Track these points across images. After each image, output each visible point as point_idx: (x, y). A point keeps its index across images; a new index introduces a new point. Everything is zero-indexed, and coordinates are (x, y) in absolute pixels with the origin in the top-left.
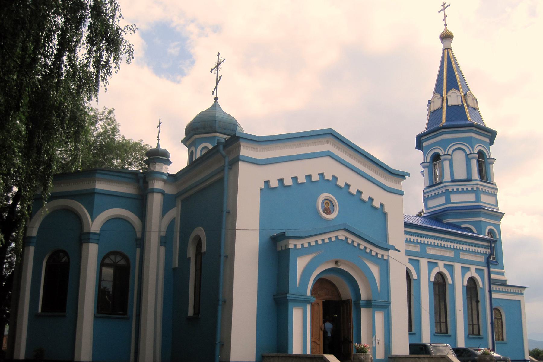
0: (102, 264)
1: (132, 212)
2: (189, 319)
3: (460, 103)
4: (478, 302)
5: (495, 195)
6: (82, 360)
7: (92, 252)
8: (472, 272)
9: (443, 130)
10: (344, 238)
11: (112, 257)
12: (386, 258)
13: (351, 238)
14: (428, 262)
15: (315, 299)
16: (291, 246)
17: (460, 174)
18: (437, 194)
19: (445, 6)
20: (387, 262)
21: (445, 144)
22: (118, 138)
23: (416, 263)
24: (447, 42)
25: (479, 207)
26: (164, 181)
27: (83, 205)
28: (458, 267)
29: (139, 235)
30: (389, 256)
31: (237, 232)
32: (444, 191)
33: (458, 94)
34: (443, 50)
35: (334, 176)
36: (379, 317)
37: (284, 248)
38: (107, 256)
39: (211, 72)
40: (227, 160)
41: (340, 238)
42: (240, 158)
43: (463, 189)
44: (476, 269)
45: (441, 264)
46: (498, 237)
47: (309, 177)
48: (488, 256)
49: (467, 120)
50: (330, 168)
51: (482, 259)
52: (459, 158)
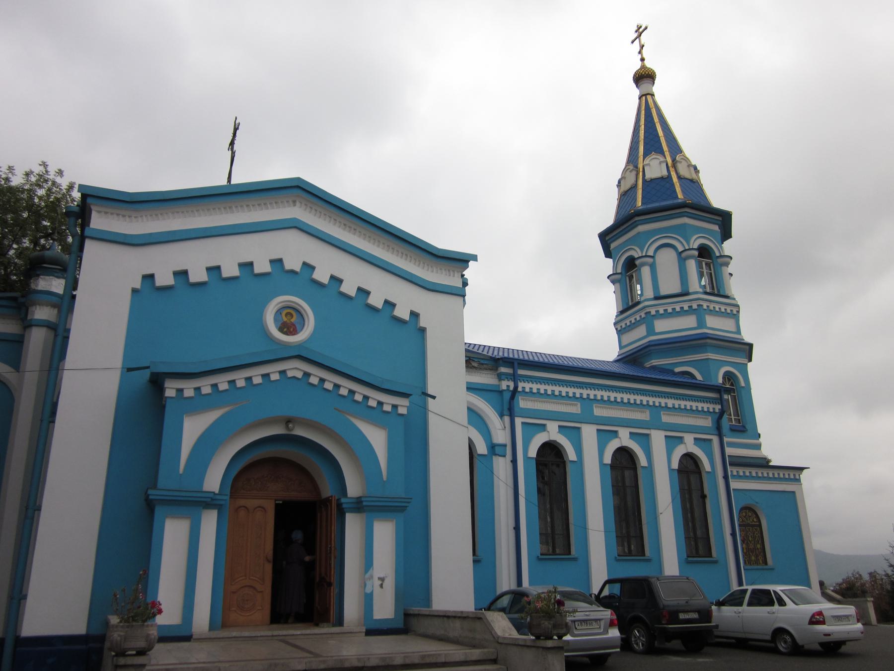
3: (665, 173)
4: (704, 497)
5: (735, 316)
6: (375, 618)
8: (689, 445)
9: (637, 219)
13: (316, 374)
14: (598, 430)
17: (670, 284)
18: (633, 321)
19: (641, 30)
21: (640, 240)
24: (645, 86)
25: (705, 337)
28: (658, 438)
32: (643, 316)
33: (662, 159)
34: (640, 98)
36: (385, 533)
41: (290, 374)
43: (674, 309)
46: (743, 384)
48: (717, 416)
50: (295, 250)
51: (707, 422)
52: (667, 261)
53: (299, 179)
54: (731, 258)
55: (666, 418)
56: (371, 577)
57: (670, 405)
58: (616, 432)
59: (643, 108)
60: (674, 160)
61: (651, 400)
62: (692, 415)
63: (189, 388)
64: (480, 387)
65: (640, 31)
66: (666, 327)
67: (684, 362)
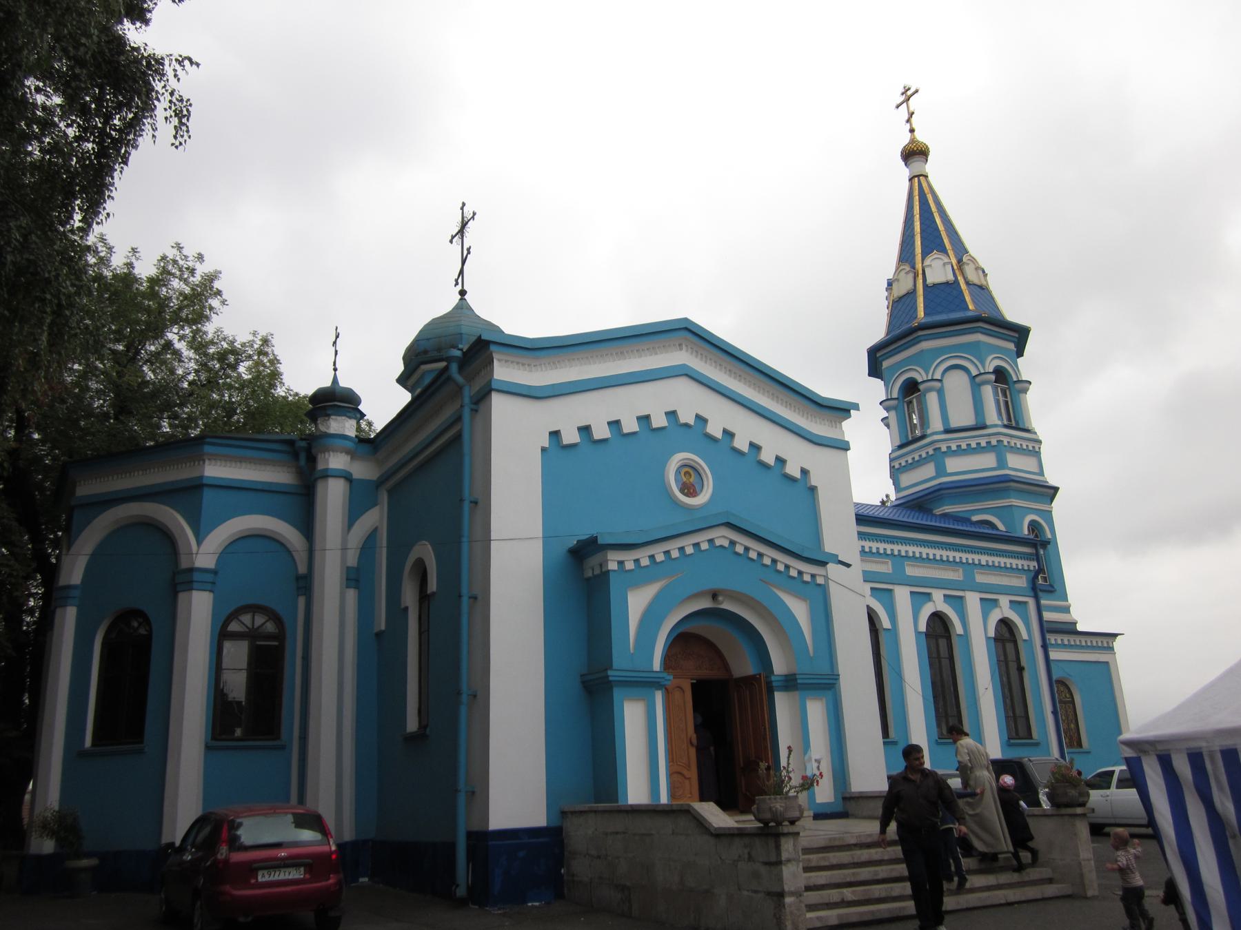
0: (222, 635)
1: (286, 521)
2: (411, 739)
3: (951, 277)
4: (1021, 669)
5: (1036, 454)
7: (199, 609)
8: (1004, 609)
9: (920, 333)
10: (726, 543)
11: (246, 618)
12: (820, 580)
13: (743, 541)
15: (671, 677)
16: (612, 566)
17: (962, 415)
18: (917, 458)
19: (909, 93)
20: (824, 590)
21: (923, 360)
22: (280, 391)
23: (885, 595)
24: (917, 166)
26: (348, 452)
27: (178, 511)
28: (973, 601)
29: (302, 569)
30: (826, 578)
31: (494, 546)
32: (931, 452)
33: (946, 260)
34: (911, 180)
35: (698, 416)
36: (816, 711)
37: (597, 572)
38: (234, 615)
39: (451, 242)
40: (468, 393)
41: (718, 543)
42: (494, 386)
44: (1011, 602)
45: (938, 595)
47: (645, 419)
48: (1032, 574)
49: (967, 308)
50: (688, 401)
51: (1021, 582)
52: (957, 385)
53: (686, 319)
54: (1030, 383)
55: (980, 578)
56: (810, 759)
57: (984, 563)
58: (929, 594)
59: (916, 193)
60: (960, 261)
61: (964, 556)
62: (1006, 572)
63: (629, 559)
64: (259, 487)
65: (908, 95)
66: (960, 467)
67: (984, 510)
